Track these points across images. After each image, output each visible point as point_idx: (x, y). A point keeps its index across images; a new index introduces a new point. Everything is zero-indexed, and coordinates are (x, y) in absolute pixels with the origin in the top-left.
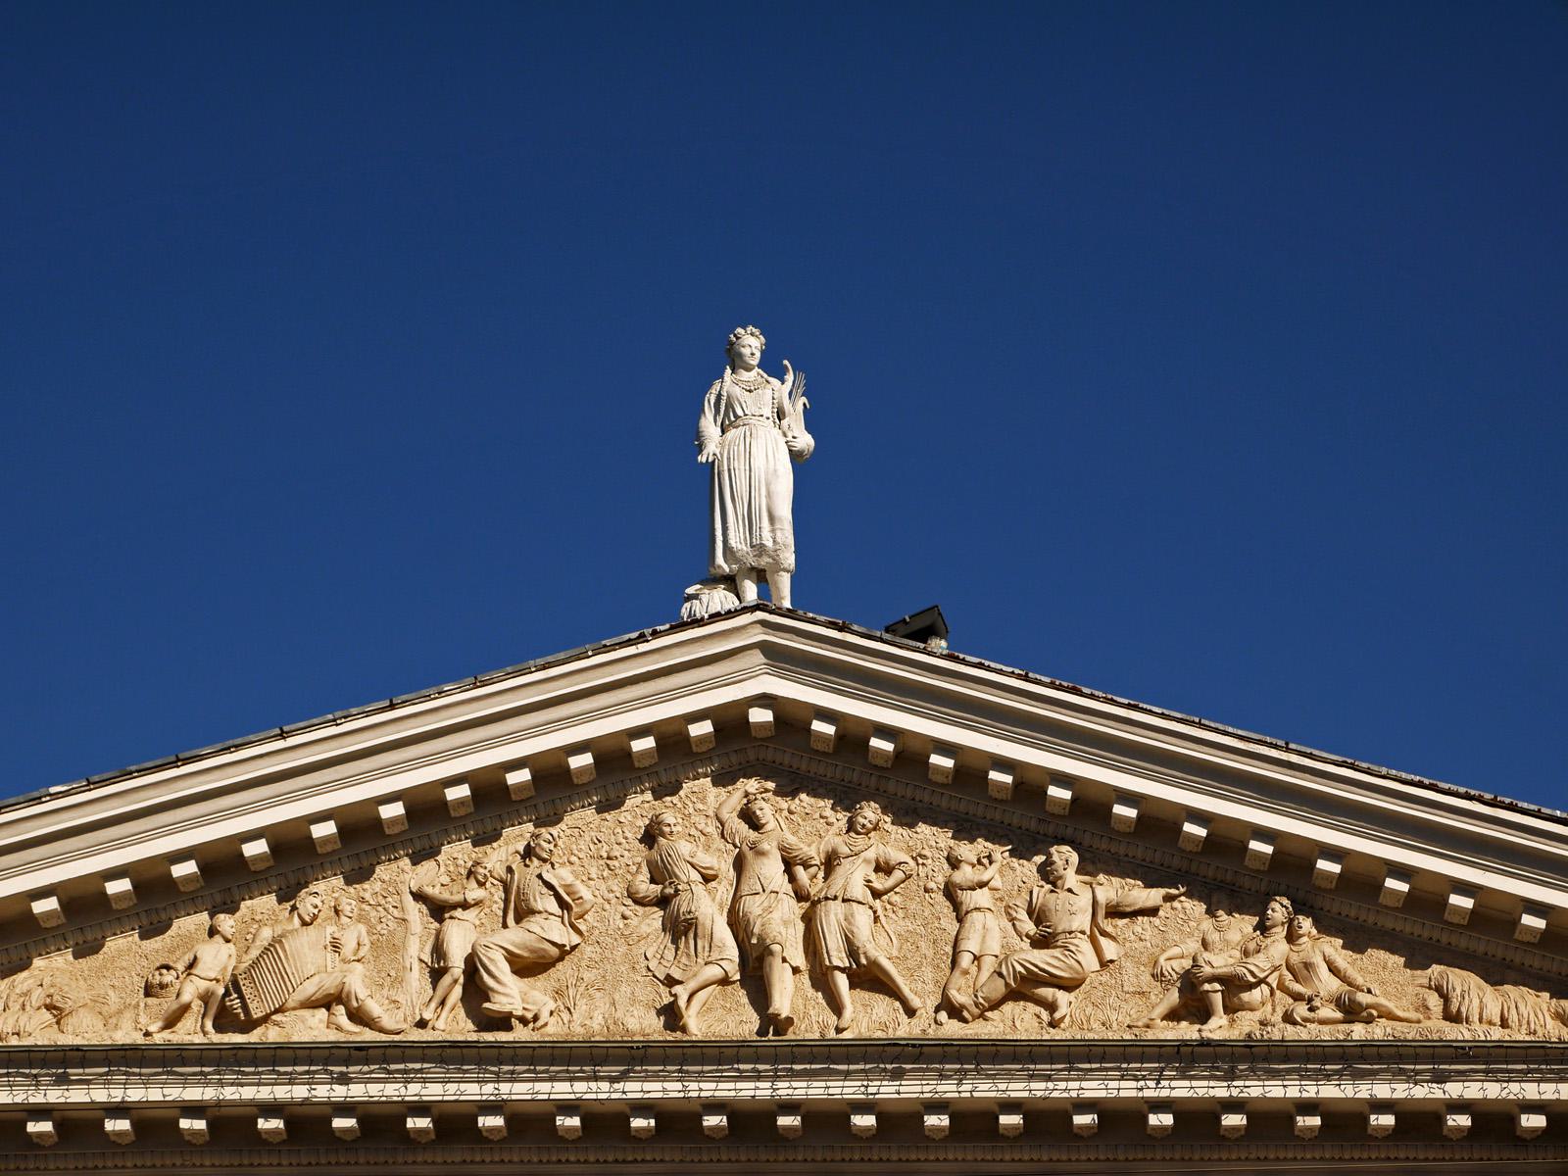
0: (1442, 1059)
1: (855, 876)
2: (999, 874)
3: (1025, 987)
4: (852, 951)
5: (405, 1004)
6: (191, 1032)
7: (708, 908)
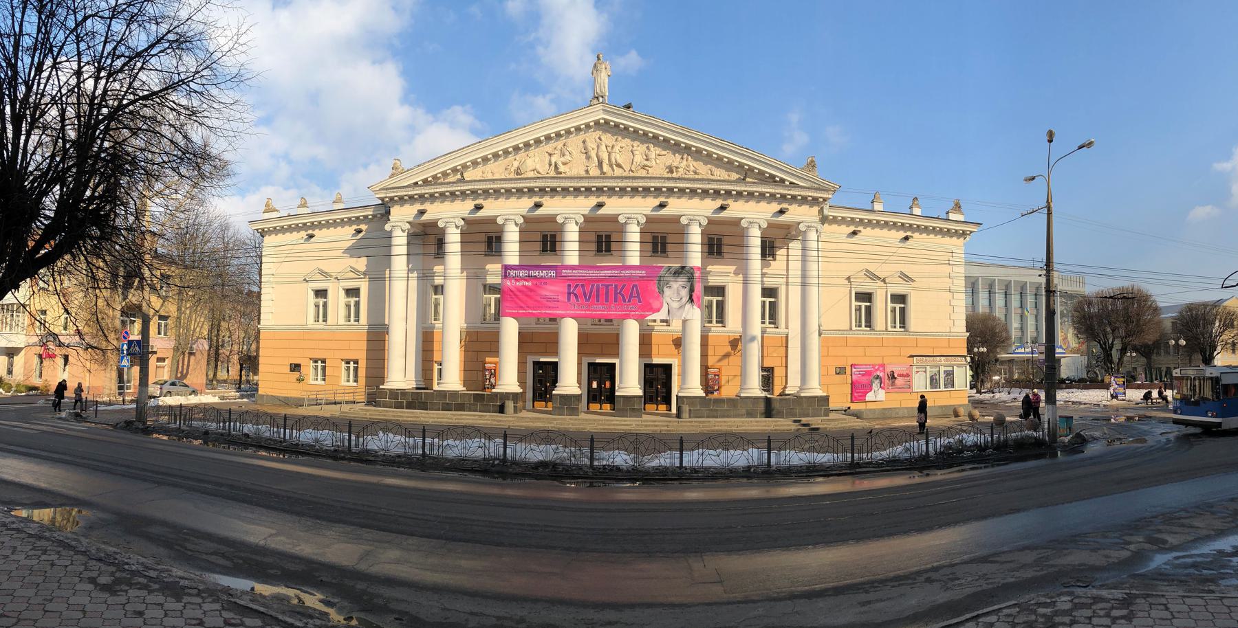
0: (709, 181)
1: (617, 149)
2: (640, 148)
3: (644, 167)
5: (544, 169)
6: (512, 176)
7: (593, 154)
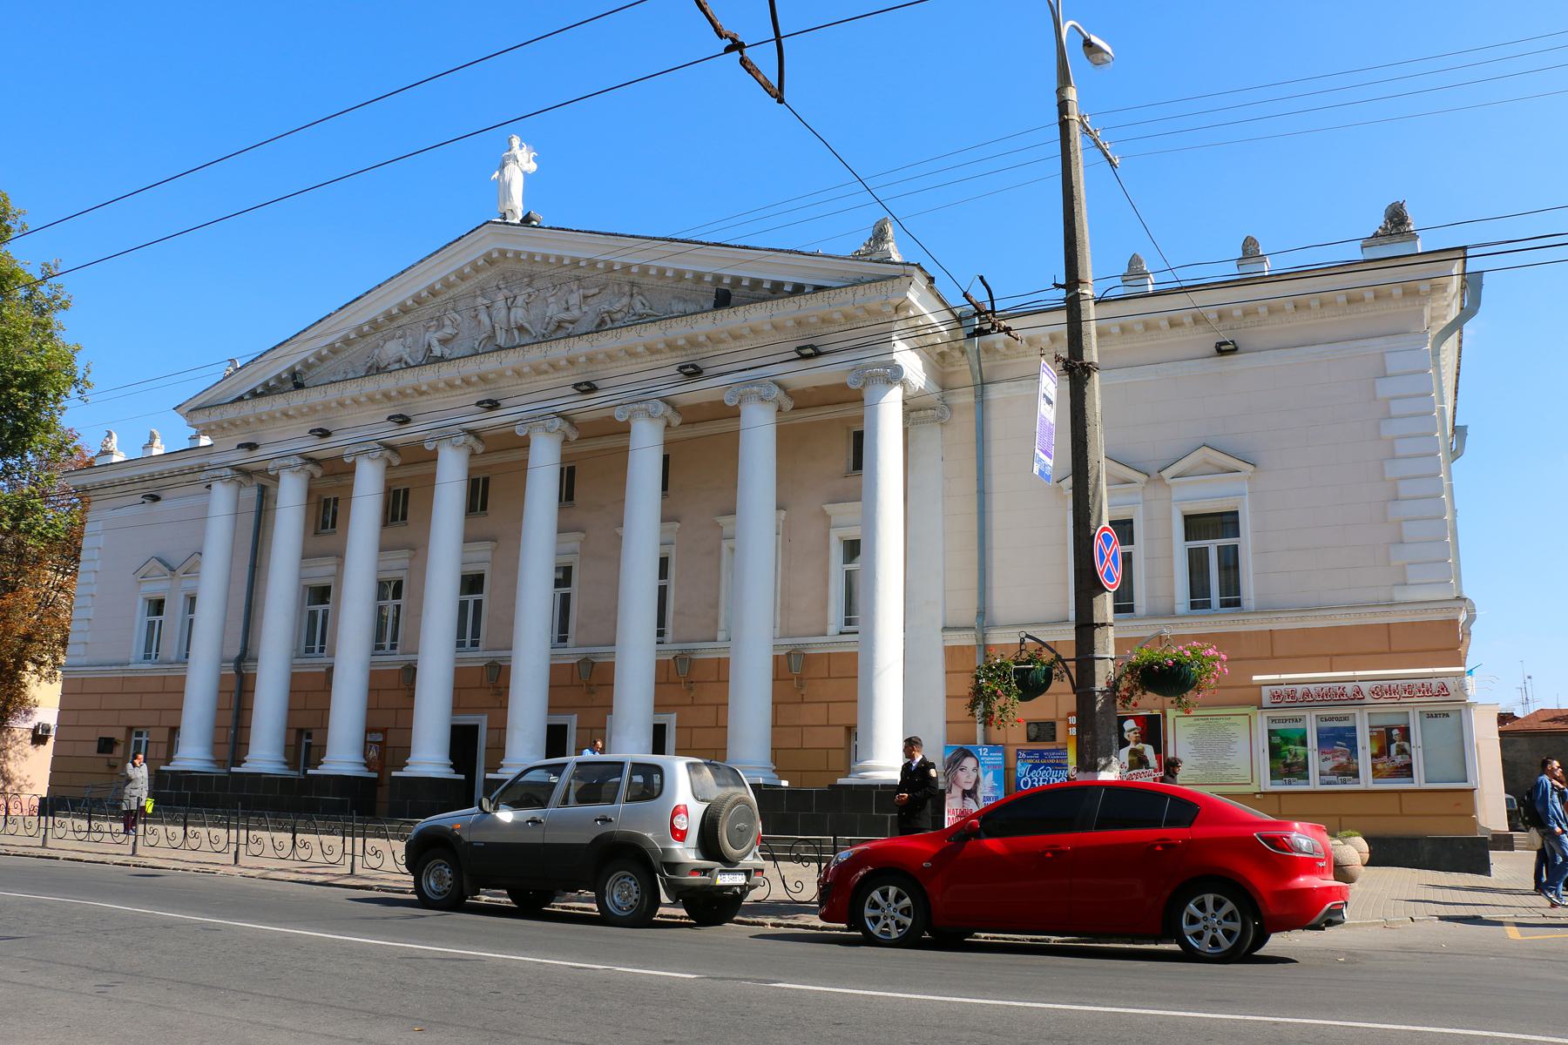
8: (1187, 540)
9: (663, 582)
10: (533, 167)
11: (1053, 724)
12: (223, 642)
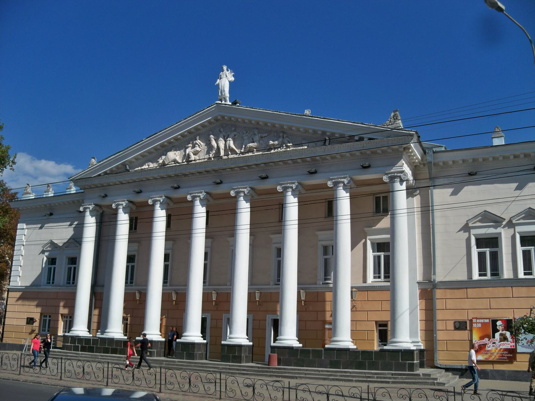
4: (229, 146)
7: (214, 143)
8: (522, 246)
9: (279, 259)
10: (232, 79)
11: (466, 322)
12: (231, 282)
